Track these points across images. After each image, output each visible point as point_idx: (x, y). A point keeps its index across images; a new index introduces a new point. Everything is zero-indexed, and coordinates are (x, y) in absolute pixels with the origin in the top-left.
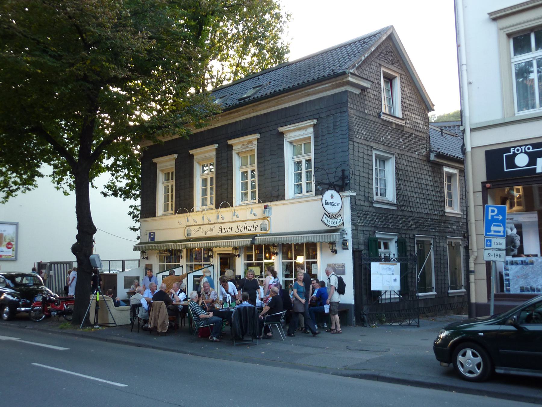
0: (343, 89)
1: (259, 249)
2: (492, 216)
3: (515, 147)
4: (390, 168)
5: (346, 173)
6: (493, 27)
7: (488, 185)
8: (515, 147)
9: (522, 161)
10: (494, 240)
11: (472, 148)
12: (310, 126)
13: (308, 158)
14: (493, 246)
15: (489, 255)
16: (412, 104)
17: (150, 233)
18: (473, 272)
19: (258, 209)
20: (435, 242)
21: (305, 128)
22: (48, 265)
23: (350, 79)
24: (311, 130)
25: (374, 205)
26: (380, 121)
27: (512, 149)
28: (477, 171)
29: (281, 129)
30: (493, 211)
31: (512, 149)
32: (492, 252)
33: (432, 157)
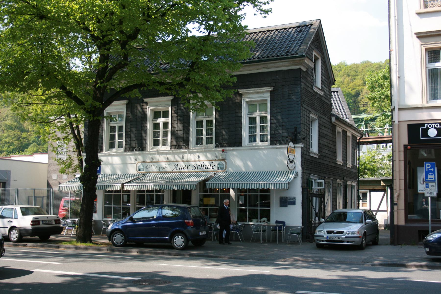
0: (297, 67)
2: (428, 169)
5: (298, 130)
6: (418, 42)
7: (409, 147)
8: (428, 124)
10: (430, 184)
11: (399, 121)
12: (268, 91)
14: (430, 187)
16: (325, 79)
18: (396, 204)
20: (333, 183)
21: (263, 93)
24: (269, 94)
25: (310, 155)
26: (313, 92)
29: (241, 91)
30: (428, 166)
32: (429, 191)
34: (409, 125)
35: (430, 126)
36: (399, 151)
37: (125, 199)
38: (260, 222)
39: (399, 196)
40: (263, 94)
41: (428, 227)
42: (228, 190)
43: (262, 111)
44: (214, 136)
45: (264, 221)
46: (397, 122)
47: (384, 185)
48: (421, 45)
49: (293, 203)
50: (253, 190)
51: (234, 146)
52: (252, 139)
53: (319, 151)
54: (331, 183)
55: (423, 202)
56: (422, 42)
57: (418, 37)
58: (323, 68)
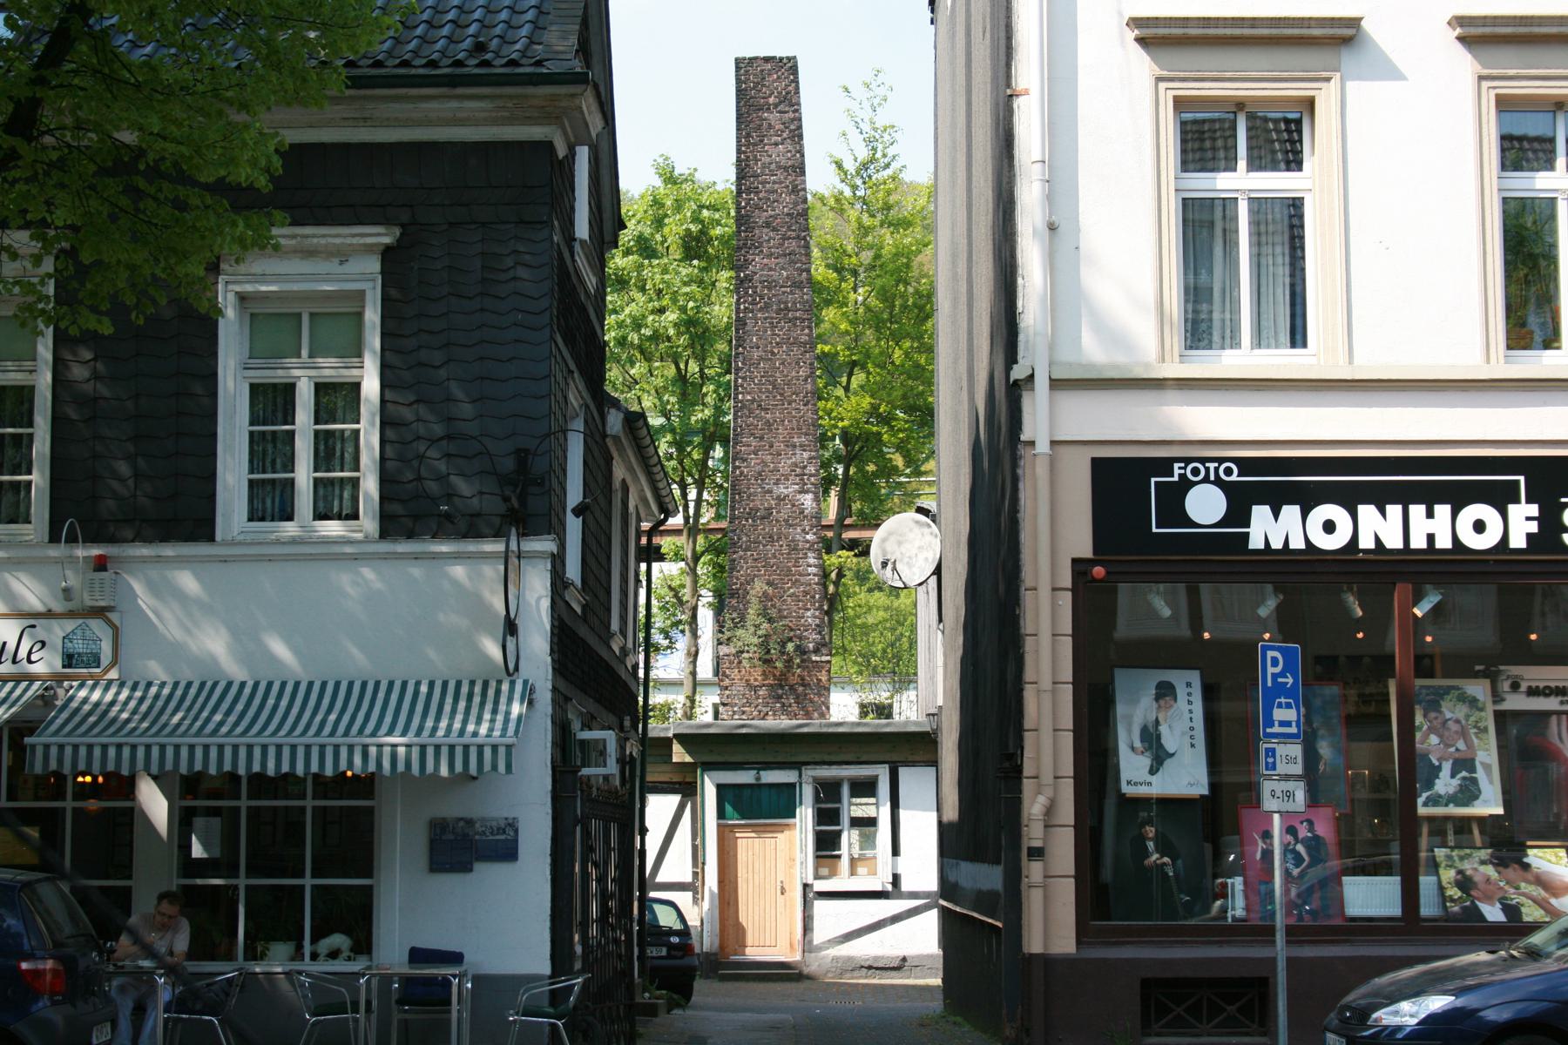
0: (536, 132)
8: (1187, 461)
9: (1206, 505)
11: (1053, 443)
12: (368, 249)
13: (331, 369)
24: (374, 265)
27: (1176, 466)
31: (1176, 466)
34: (1097, 464)
35: (1196, 472)
36: (1054, 589)
38: (314, 956)
39: (1049, 811)
40: (344, 264)
41: (1274, 960)
42: (125, 786)
43: (326, 354)
45: (334, 955)
46: (1043, 447)
47: (688, 759)
48: (1481, 78)
49: (508, 852)
50: (285, 784)
52: (271, 501)
54: (612, 748)
55: (1142, 839)
56: (1484, 66)
57: (1141, 41)
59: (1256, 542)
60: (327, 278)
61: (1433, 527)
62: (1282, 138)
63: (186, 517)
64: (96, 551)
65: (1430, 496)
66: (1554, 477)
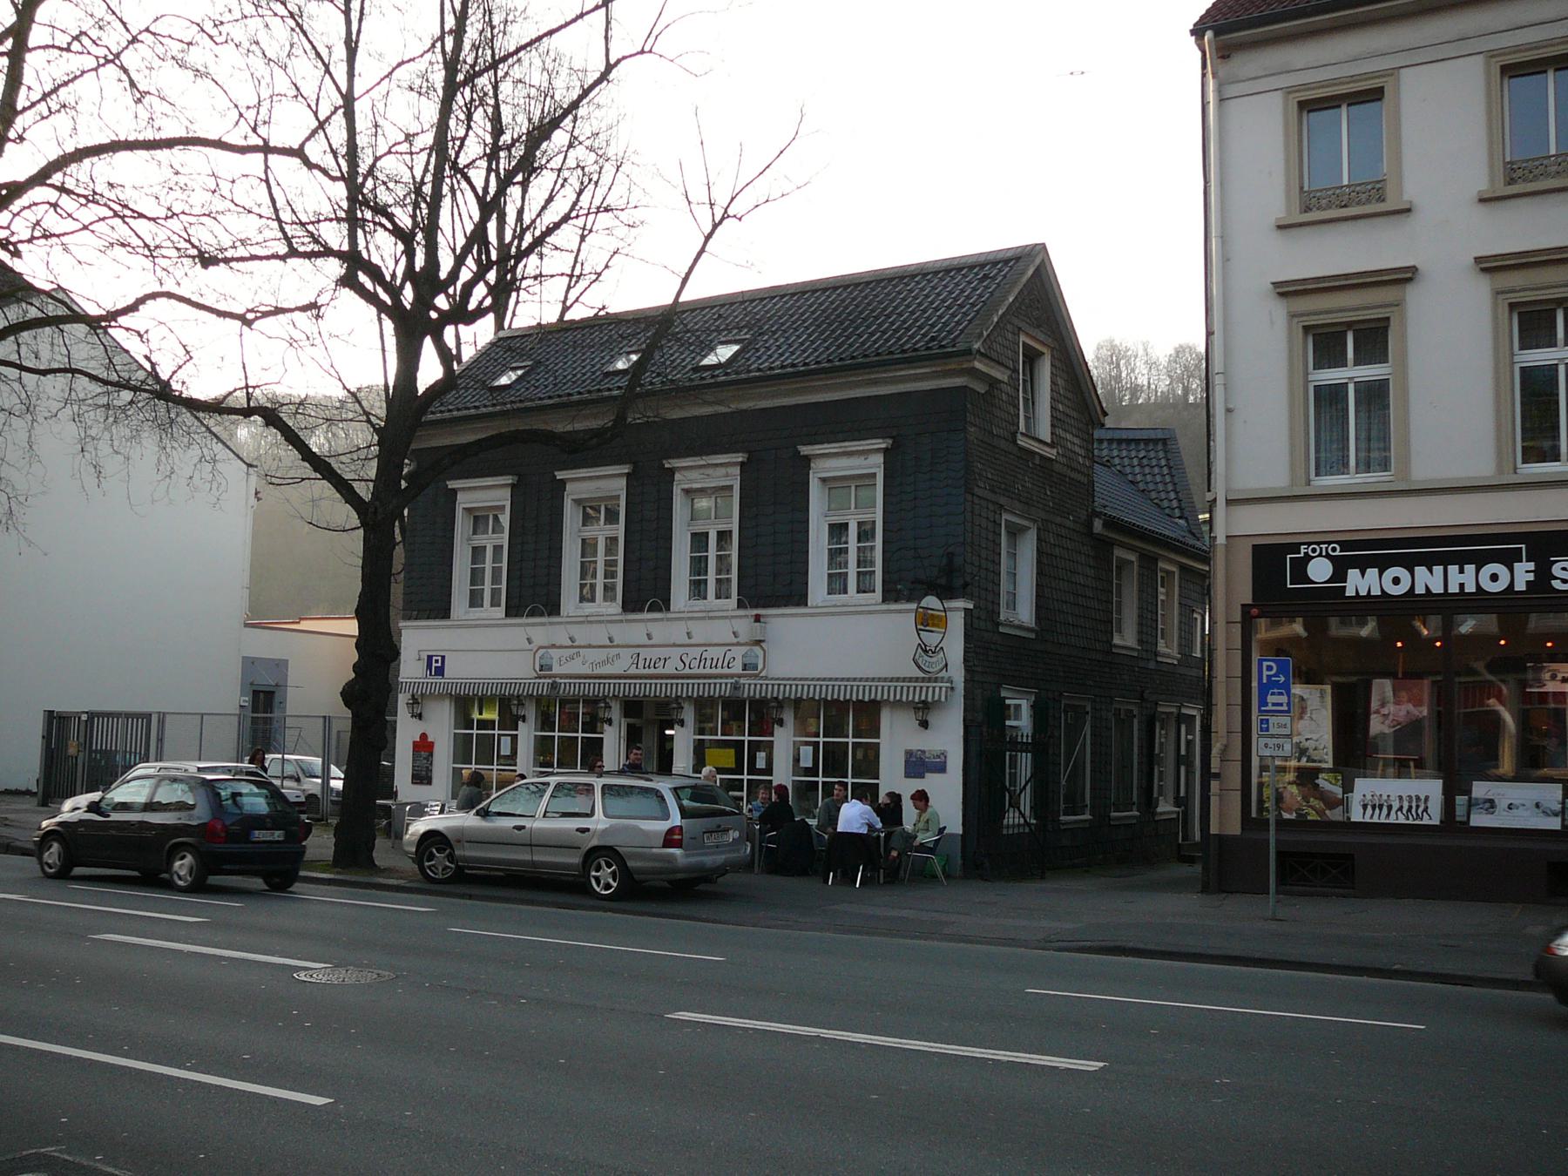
1: (748, 713)
3: (1309, 544)
4: (1028, 550)
6: (1279, 310)
8: (1309, 544)
9: (1320, 570)
10: (1273, 720)
12: (878, 450)
15: (1266, 745)
16: (1068, 411)
17: (430, 658)
18: (1217, 776)
19: (743, 624)
20: (1094, 708)
21: (865, 453)
22: (84, 717)
23: (977, 365)
24: (880, 459)
25: (1001, 629)
28: (1234, 583)
29: (805, 450)
30: (1269, 668)
32: (1271, 742)
33: (1098, 525)
37: (506, 751)
39: (1225, 749)
40: (863, 460)
44: (734, 575)
46: (1221, 540)
51: (779, 606)
53: (1038, 618)
54: (1089, 709)
58: (1060, 381)
59: (1350, 592)
60: (859, 467)
61: (1463, 579)
62: (1374, 339)
63: (795, 595)
64: (755, 612)
65: (1461, 560)
66: (1546, 544)
